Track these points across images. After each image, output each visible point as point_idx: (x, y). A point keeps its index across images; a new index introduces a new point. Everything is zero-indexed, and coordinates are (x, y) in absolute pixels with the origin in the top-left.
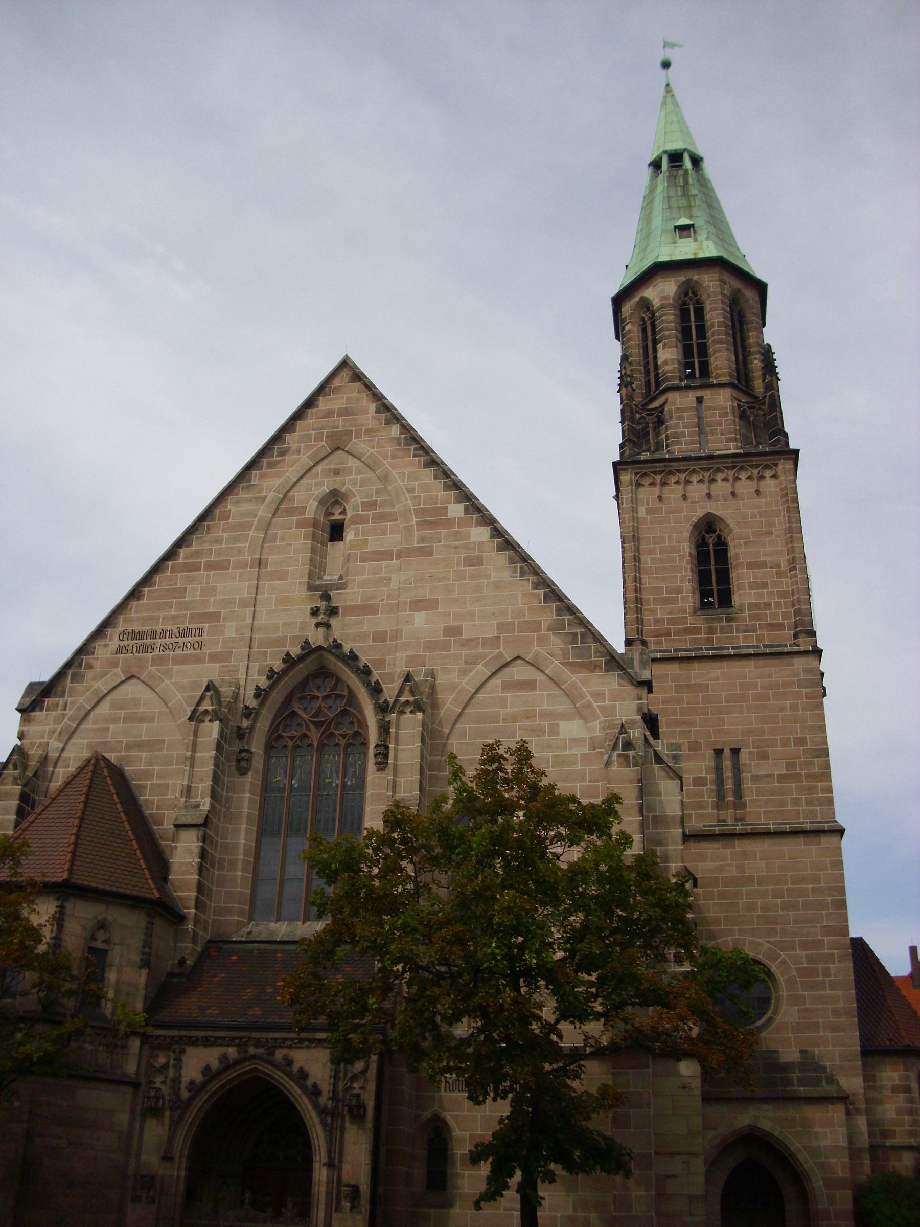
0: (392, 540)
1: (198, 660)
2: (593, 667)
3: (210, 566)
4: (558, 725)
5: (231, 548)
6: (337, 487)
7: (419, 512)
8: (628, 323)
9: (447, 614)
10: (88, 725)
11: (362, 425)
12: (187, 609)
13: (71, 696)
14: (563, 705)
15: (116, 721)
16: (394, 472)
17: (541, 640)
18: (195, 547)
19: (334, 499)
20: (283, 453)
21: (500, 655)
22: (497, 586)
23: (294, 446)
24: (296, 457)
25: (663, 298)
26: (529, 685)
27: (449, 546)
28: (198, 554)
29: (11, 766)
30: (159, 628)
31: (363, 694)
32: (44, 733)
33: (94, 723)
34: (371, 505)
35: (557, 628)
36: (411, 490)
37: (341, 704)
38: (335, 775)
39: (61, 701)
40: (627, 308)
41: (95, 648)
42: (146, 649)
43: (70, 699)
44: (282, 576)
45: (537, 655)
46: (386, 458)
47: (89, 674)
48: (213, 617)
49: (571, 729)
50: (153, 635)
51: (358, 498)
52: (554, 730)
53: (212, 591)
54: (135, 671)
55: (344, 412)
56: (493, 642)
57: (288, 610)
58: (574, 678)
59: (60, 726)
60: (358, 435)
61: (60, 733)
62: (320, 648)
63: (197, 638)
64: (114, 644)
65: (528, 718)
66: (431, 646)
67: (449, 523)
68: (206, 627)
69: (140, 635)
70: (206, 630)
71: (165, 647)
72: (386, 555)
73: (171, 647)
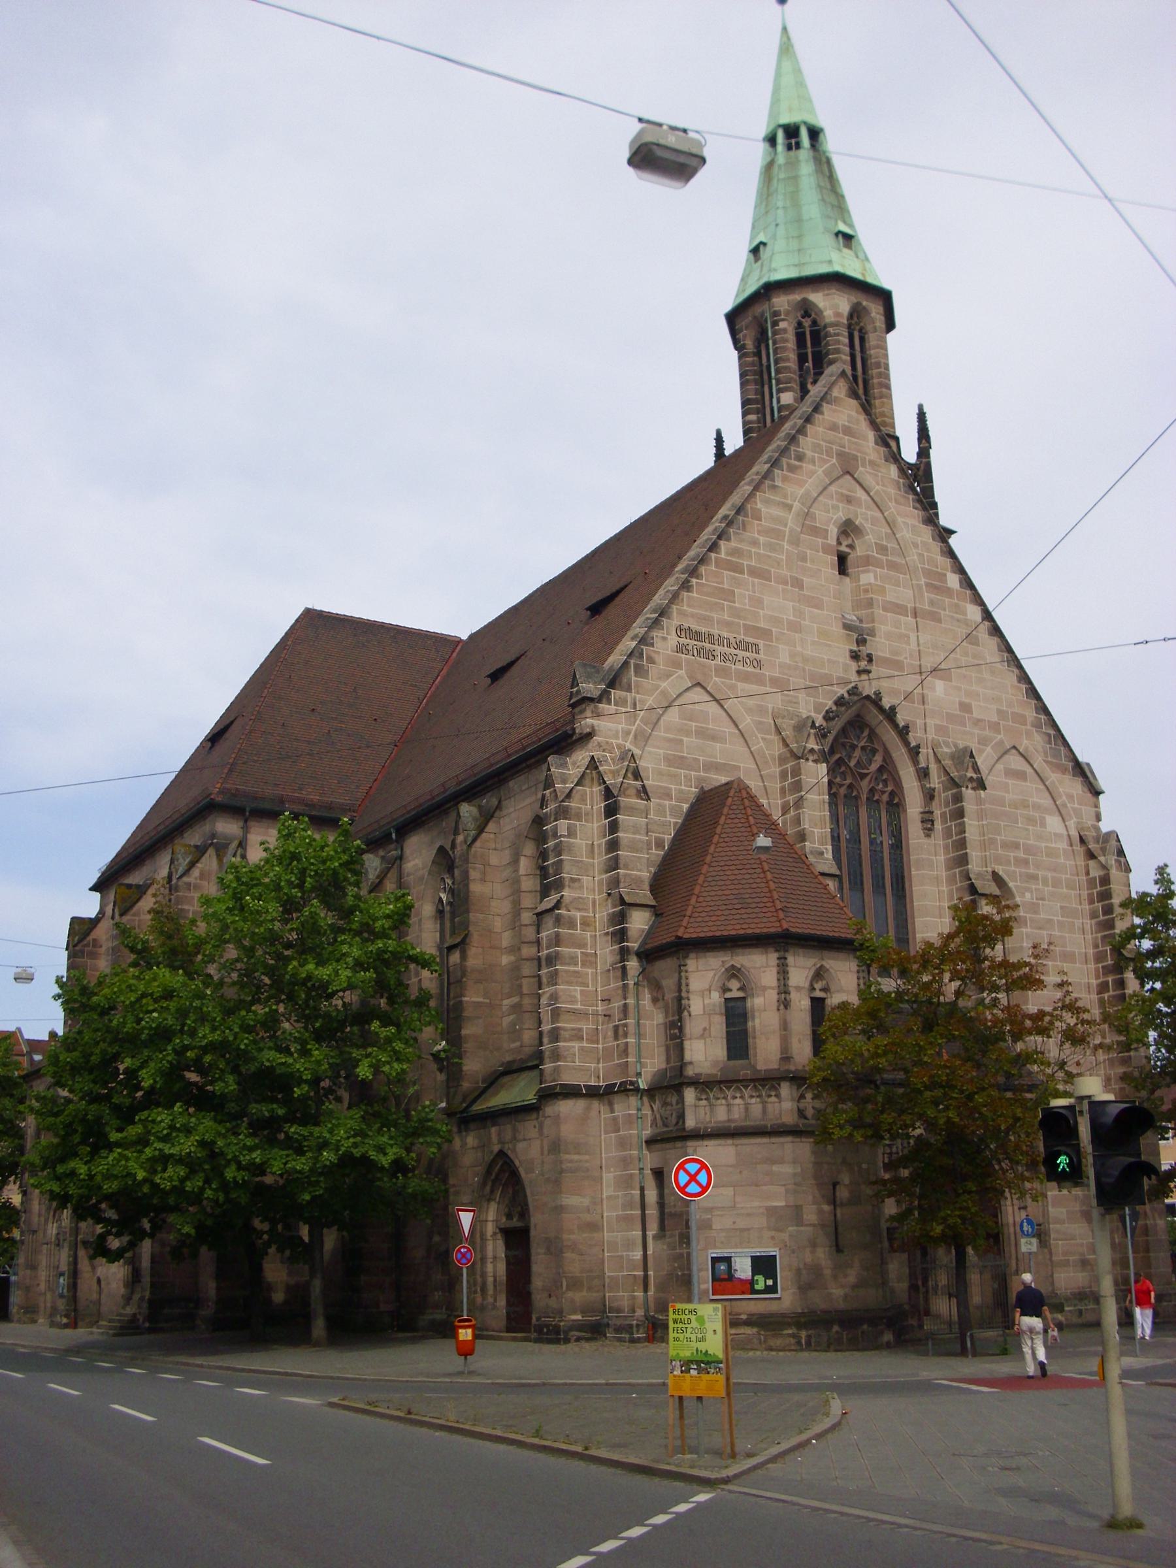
0: (904, 595)
1: (760, 681)
2: (1064, 771)
3: (753, 572)
4: (1044, 818)
5: (770, 557)
6: (851, 516)
7: (928, 573)
8: (783, 320)
9: (959, 689)
10: (660, 733)
11: (866, 453)
12: (739, 617)
13: (638, 693)
14: (1046, 801)
15: (688, 733)
16: (900, 520)
17: (1029, 735)
18: (733, 544)
19: (848, 529)
20: (800, 457)
21: (1001, 742)
23: (809, 453)
24: (811, 467)
25: (838, 314)
26: (1021, 775)
27: (952, 617)
28: (736, 552)
29: (629, 775)
30: (715, 632)
31: (900, 756)
32: (617, 732)
33: (668, 730)
34: (883, 549)
35: (1037, 725)
36: (916, 545)
37: (878, 760)
38: (878, 832)
39: (629, 697)
40: (781, 302)
41: (653, 638)
43: (638, 696)
44: (818, 605)
45: (1026, 749)
46: (890, 500)
47: (653, 670)
48: (766, 634)
49: (1054, 823)
50: (711, 638)
51: (871, 536)
52: (1043, 824)
53: (759, 602)
54: (700, 678)
55: (848, 431)
56: (995, 727)
58: (1053, 777)
59: (634, 728)
60: (864, 465)
61: (635, 737)
62: (868, 697)
63: (755, 655)
64: (673, 640)
65: (1025, 807)
66: (951, 717)
67: (948, 592)
68: (761, 643)
69: (696, 635)
70: (761, 647)
71: (725, 658)
72: (899, 609)
73: (731, 659)
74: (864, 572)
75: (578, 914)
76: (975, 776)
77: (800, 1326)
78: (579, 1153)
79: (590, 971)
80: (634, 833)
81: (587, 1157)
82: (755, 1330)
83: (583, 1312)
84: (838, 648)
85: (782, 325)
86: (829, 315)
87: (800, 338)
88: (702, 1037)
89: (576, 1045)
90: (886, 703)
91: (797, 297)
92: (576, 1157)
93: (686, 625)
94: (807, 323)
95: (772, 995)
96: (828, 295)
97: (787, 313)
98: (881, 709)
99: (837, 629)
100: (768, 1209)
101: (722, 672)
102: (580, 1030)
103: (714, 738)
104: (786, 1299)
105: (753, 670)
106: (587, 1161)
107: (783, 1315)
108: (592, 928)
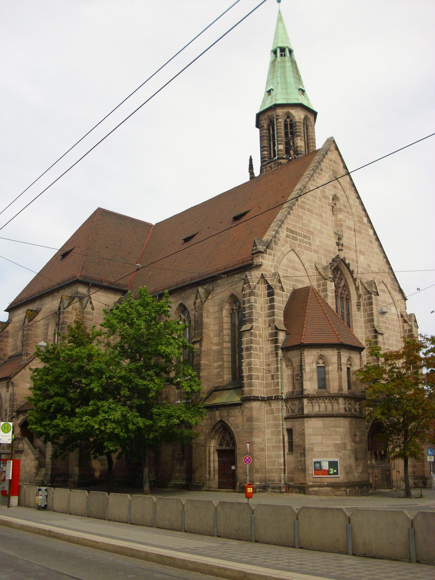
3: (309, 210)
8: (280, 118)
22: (376, 253)
28: (303, 202)
39: (272, 252)
42: (296, 239)
54: (293, 248)
57: (330, 239)
74: (340, 214)
75: (258, 332)
76: (375, 291)
77: (347, 487)
78: (258, 422)
79: (261, 354)
80: (279, 303)
81: (261, 423)
82: (330, 488)
83: (260, 481)
84: (333, 240)
85: (280, 120)
86: (297, 118)
87: (286, 126)
88: (310, 380)
89: (257, 381)
90: (347, 262)
91: (285, 110)
92: (257, 423)
93: (289, 227)
94: (288, 120)
95: (336, 366)
96: (297, 111)
97: (282, 116)
98: (345, 263)
99: (332, 234)
100: (335, 444)
101: (300, 246)
102: (258, 376)
103: (297, 270)
104: (341, 477)
105: (309, 246)
106: (261, 425)
107: (340, 483)
108: (262, 338)
